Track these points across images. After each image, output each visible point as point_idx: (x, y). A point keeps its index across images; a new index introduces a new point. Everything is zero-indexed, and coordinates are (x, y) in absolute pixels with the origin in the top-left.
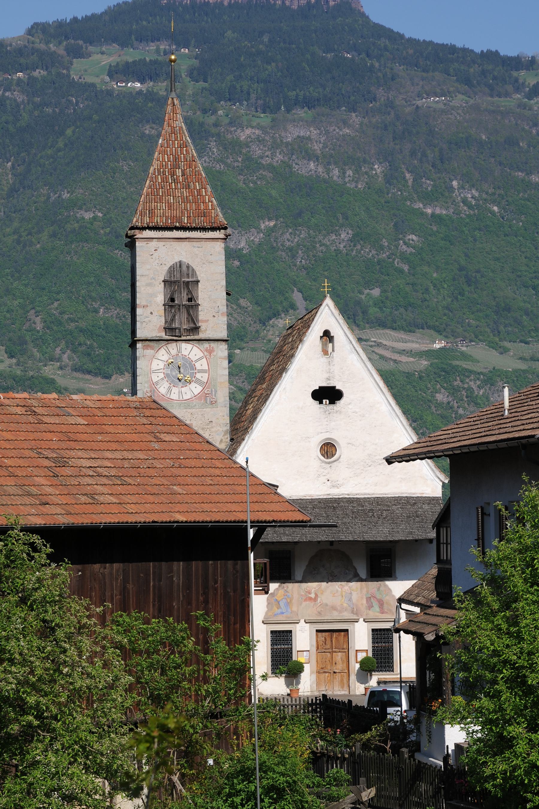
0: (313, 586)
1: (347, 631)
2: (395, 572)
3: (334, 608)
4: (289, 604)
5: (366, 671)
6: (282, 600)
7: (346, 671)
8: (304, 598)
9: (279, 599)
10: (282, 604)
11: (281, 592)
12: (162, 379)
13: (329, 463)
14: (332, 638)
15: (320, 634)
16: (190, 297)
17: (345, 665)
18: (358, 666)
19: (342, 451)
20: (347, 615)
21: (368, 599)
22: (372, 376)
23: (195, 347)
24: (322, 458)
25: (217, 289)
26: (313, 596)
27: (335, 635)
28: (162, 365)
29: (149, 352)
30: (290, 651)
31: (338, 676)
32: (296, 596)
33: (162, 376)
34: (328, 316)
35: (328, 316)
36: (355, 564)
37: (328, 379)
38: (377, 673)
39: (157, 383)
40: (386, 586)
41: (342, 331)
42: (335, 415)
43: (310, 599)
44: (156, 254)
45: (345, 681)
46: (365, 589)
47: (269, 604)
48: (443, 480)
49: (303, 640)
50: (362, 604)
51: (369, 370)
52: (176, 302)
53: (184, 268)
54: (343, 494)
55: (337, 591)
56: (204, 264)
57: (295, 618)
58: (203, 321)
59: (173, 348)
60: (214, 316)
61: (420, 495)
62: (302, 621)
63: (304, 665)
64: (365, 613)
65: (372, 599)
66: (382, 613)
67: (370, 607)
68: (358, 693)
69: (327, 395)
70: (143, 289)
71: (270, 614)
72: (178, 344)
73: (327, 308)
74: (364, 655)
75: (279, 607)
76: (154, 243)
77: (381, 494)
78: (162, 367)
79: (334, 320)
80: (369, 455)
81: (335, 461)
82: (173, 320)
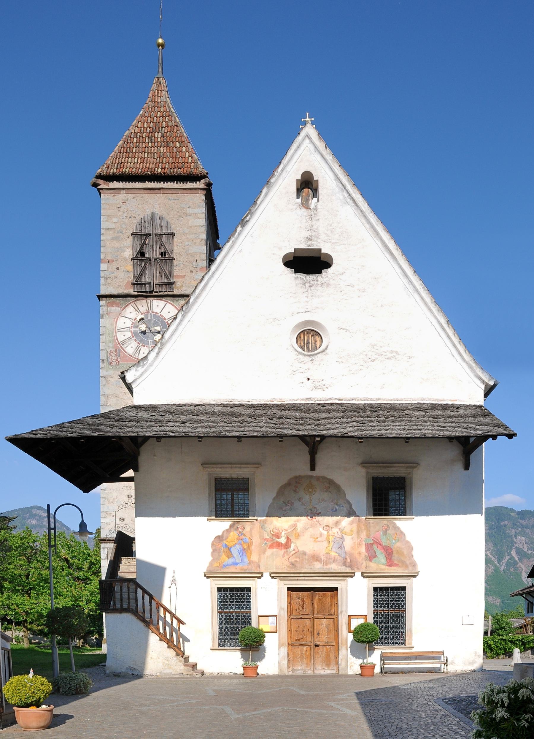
0: (283, 523)
1: (336, 589)
2: (411, 494)
3: (315, 558)
4: (246, 551)
5: (363, 642)
6: (235, 545)
7: (334, 644)
8: (269, 543)
9: (230, 544)
10: (235, 551)
11: (234, 535)
12: (130, 338)
13: (310, 356)
14: (313, 600)
15: (294, 594)
16: (163, 251)
17: (332, 636)
18: (351, 637)
19: (331, 338)
20: (335, 567)
21: (369, 546)
22: (377, 234)
23: (168, 304)
24: (296, 346)
25: (195, 243)
26: (283, 540)
27: (317, 595)
28: (129, 323)
29: (114, 309)
30: (247, 618)
31: (322, 651)
32: (256, 540)
33: (129, 334)
34: (308, 152)
35: (308, 152)
36: (349, 497)
37: (309, 239)
38: (379, 647)
39: (123, 342)
40: (396, 528)
41: (331, 174)
42: (319, 288)
43: (279, 545)
44: (124, 208)
45: (332, 657)
46: (365, 533)
47: (214, 551)
48: (486, 380)
49: (268, 601)
50: (360, 553)
51: (372, 226)
52: (147, 256)
53: (158, 221)
54: (331, 399)
55: (321, 535)
56: (180, 216)
57: (255, 571)
58: (178, 277)
59: (143, 304)
60: (191, 271)
61: (450, 403)
62: (266, 575)
63: (266, 634)
64: (364, 566)
65: (375, 547)
66: (390, 565)
67: (372, 557)
68: (350, 672)
69: (308, 263)
70: (108, 243)
71: (215, 565)
72: (149, 301)
73: (307, 141)
74: (362, 621)
75: (229, 554)
76: (122, 195)
77: (391, 400)
78: (130, 326)
79: (319, 157)
80: (373, 346)
81: (320, 353)
82: (141, 274)
